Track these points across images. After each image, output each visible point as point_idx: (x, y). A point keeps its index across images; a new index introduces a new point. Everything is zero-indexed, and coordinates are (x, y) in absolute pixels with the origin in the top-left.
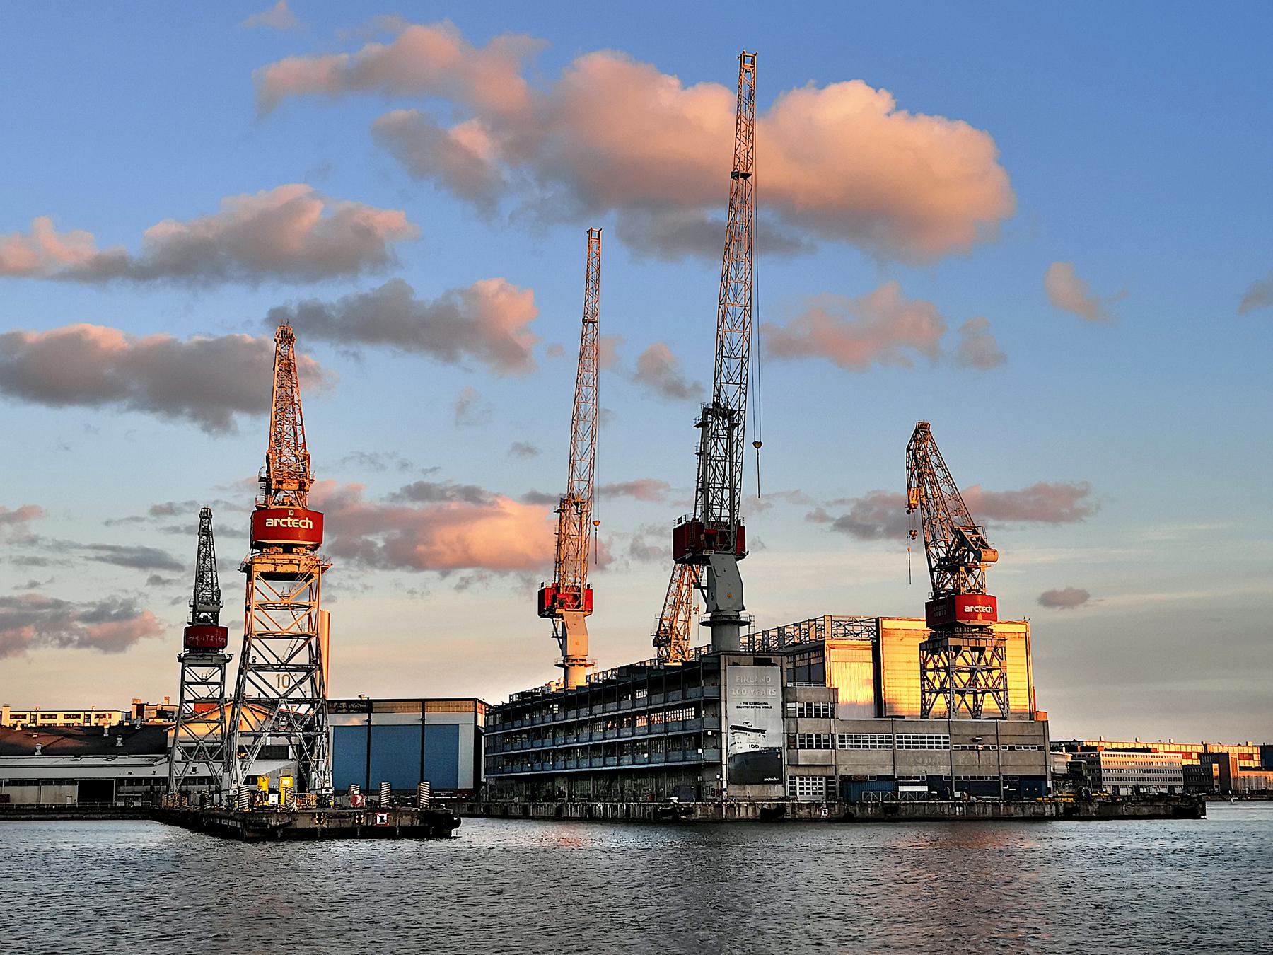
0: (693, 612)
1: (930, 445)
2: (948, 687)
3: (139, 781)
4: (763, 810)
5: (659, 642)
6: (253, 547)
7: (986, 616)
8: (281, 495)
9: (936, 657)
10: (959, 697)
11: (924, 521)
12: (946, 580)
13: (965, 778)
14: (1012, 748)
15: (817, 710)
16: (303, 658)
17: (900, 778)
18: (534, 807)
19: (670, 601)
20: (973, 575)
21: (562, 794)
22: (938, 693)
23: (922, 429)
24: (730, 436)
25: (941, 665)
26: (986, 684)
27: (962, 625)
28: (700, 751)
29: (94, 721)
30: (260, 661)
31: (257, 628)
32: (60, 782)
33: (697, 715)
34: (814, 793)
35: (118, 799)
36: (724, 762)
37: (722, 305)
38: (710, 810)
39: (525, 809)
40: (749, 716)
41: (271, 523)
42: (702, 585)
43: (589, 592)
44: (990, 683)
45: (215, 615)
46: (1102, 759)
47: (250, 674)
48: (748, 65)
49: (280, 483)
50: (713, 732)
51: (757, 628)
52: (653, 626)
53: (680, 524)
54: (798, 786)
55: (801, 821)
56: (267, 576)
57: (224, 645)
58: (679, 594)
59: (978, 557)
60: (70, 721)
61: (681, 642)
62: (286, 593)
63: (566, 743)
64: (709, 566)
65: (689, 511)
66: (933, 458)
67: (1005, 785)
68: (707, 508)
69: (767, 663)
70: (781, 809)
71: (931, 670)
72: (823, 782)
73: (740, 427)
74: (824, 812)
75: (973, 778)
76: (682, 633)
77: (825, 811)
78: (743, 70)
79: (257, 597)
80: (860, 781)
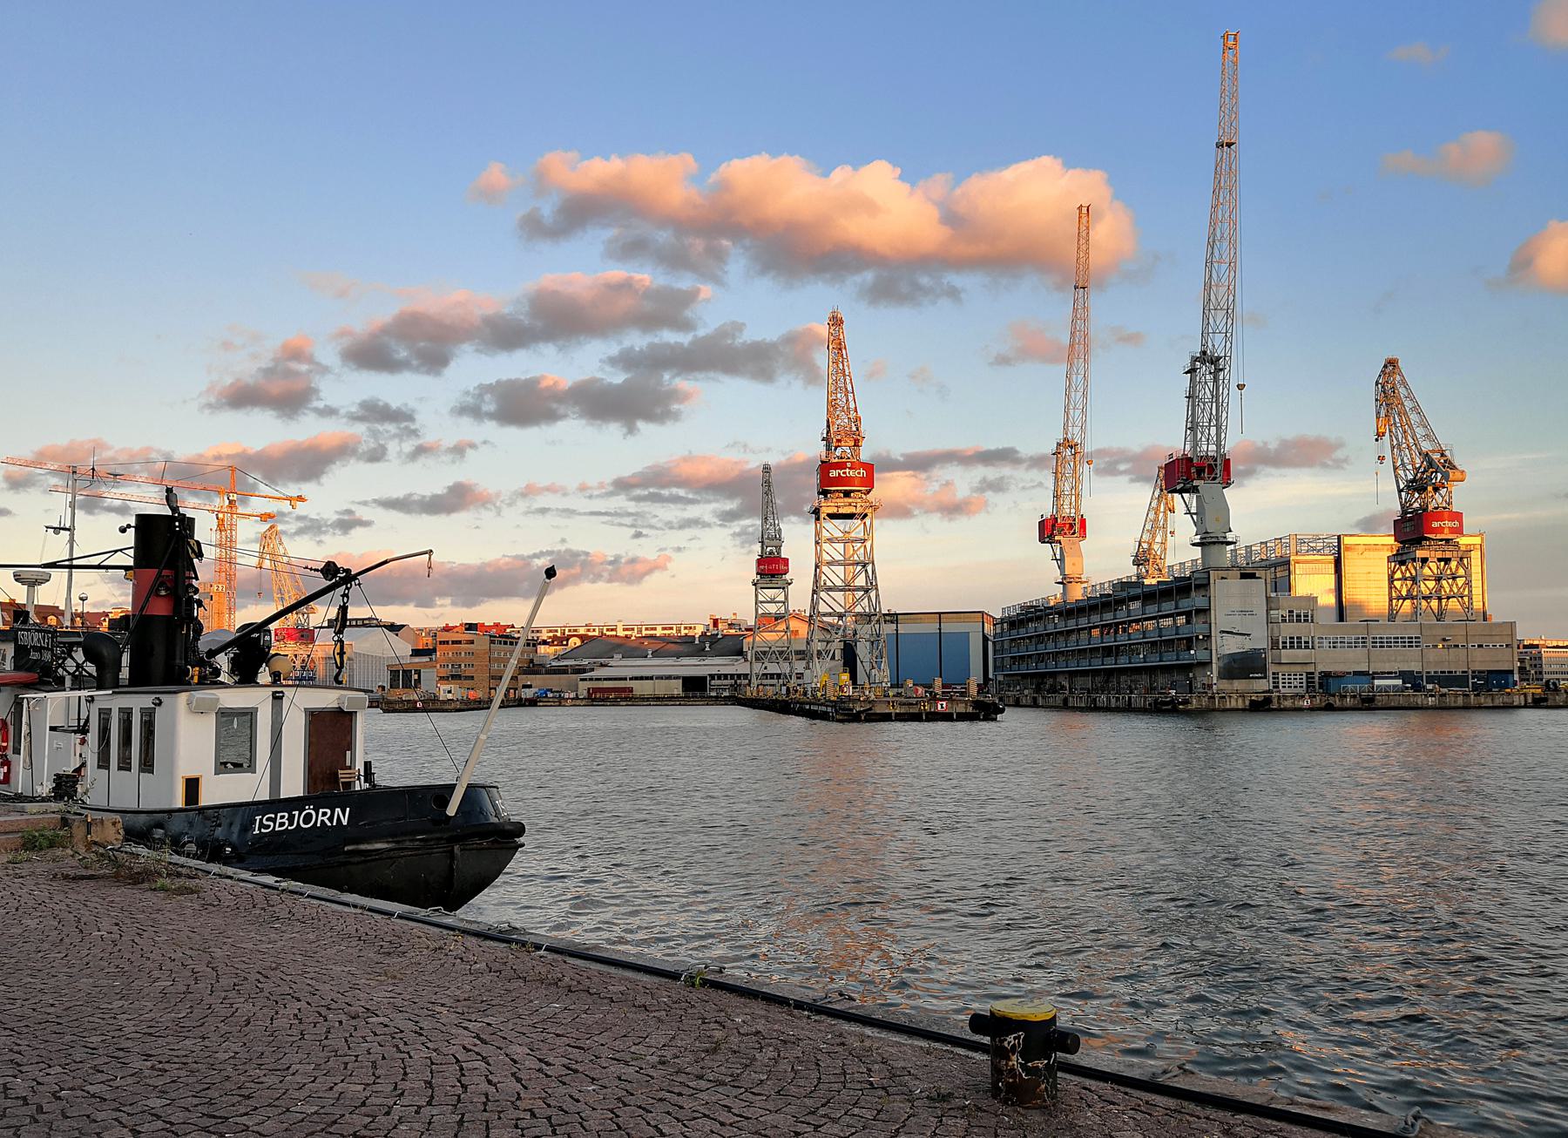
0: (1169, 535)
1: (1398, 378)
2: (1415, 593)
3: (726, 676)
4: (1251, 701)
5: (1137, 563)
6: (819, 493)
7: (1453, 531)
8: (839, 450)
9: (1403, 568)
10: (1424, 603)
11: (1393, 448)
13: (1449, 672)
14: (1480, 646)
15: (1299, 616)
16: (861, 581)
17: (1374, 673)
18: (1043, 697)
19: (1148, 527)
21: (1063, 687)
22: (1404, 599)
23: (1392, 363)
24: (1216, 380)
25: (1408, 575)
26: (1451, 590)
27: (1429, 539)
28: (1192, 652)
29: (683, 632)
30: (829, 583)
31: (826, 557)
32: (669, 677)
33: (1188, 622)
34: (1295, 687)
35: (711, 690)
36: (1214, 661)
37: (1209, 263)
38: (1205, 701)
39: (1035, 699)
40: (1237, 623)
41: (834, 473)
43: (1083, 522)
44: (1456, 590)
45: (779, 548)
46: (1544, 655)
47: (823, 594)
48: (1231, 42)
49: (839, 441)
51: (1242, 544)
52: (1133, 549)
54: (1281, 681)
55: (1286, 710)
56: (832, 516)
57: (786, 572)
58: (1156, 520)
59: (1446, 477)
60: (667, 632)
61: (1158, 561)
62: (847, 529)
63: (1066, 647)
66: (1402, 391)
67: (1473, 678)
68: (1195, 444)
69: (1252, 576)
70: (1268, 700)
71: (1398, 580)
72: (1304, 677)
73: (1226, 371)
74: (1306, 703)
76: (1159, 553)
78: (1226, 48)
79: (825, 534)
80: (1340, 676)
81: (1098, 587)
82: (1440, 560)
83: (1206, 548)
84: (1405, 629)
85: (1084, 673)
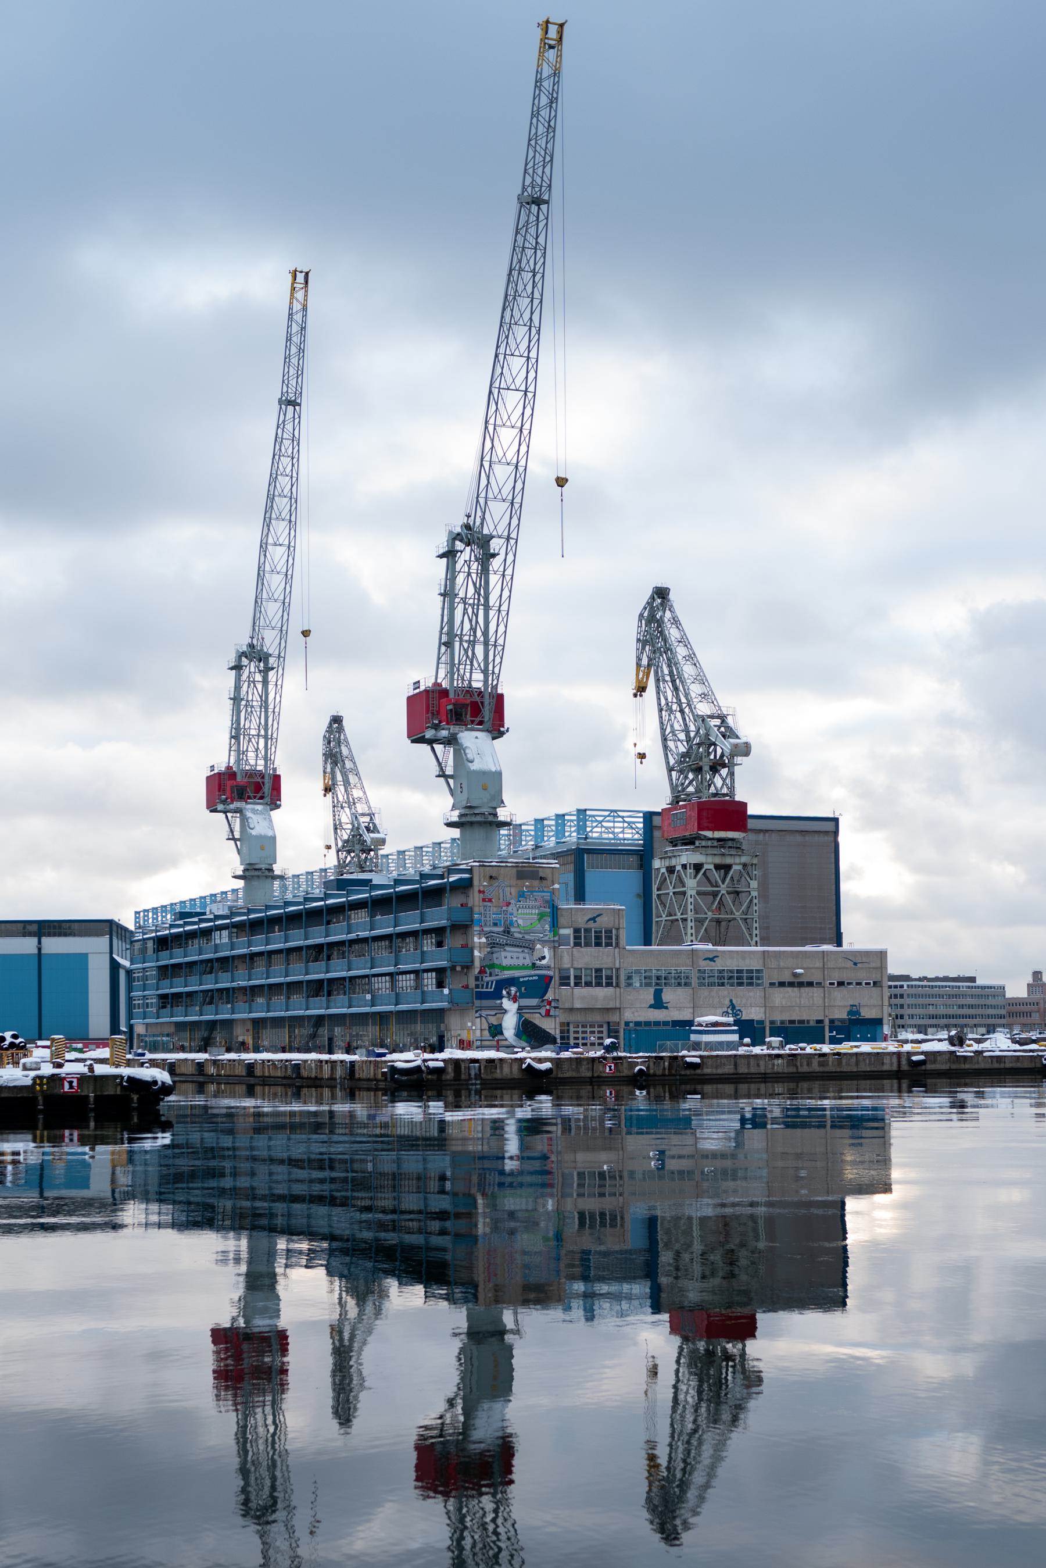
12: (687, 782)
14: (841, 984)
20: (720, 775)
24: (265, 682)
42: (447, 773)
50: (463, 967)
53: (417, 691)
54: (572, 1035)
64: (457, 747)
65: (221, 758)
75: (792, 1022)
77: (610, 1067)
81: (303, 879)
82: (718, 867)
83: (255, 883)
84: (744, 959)
85: (277, 1022)
